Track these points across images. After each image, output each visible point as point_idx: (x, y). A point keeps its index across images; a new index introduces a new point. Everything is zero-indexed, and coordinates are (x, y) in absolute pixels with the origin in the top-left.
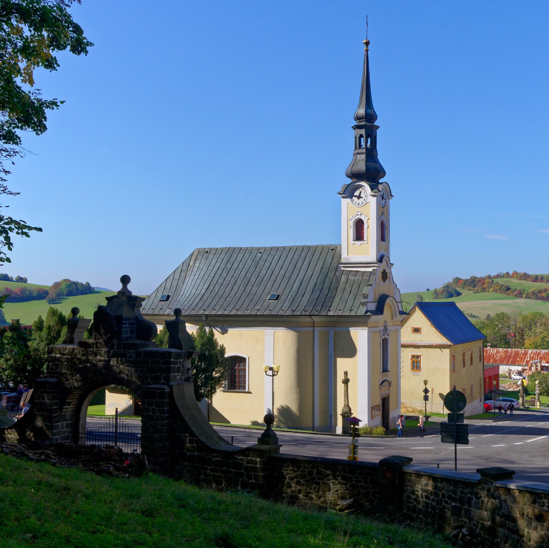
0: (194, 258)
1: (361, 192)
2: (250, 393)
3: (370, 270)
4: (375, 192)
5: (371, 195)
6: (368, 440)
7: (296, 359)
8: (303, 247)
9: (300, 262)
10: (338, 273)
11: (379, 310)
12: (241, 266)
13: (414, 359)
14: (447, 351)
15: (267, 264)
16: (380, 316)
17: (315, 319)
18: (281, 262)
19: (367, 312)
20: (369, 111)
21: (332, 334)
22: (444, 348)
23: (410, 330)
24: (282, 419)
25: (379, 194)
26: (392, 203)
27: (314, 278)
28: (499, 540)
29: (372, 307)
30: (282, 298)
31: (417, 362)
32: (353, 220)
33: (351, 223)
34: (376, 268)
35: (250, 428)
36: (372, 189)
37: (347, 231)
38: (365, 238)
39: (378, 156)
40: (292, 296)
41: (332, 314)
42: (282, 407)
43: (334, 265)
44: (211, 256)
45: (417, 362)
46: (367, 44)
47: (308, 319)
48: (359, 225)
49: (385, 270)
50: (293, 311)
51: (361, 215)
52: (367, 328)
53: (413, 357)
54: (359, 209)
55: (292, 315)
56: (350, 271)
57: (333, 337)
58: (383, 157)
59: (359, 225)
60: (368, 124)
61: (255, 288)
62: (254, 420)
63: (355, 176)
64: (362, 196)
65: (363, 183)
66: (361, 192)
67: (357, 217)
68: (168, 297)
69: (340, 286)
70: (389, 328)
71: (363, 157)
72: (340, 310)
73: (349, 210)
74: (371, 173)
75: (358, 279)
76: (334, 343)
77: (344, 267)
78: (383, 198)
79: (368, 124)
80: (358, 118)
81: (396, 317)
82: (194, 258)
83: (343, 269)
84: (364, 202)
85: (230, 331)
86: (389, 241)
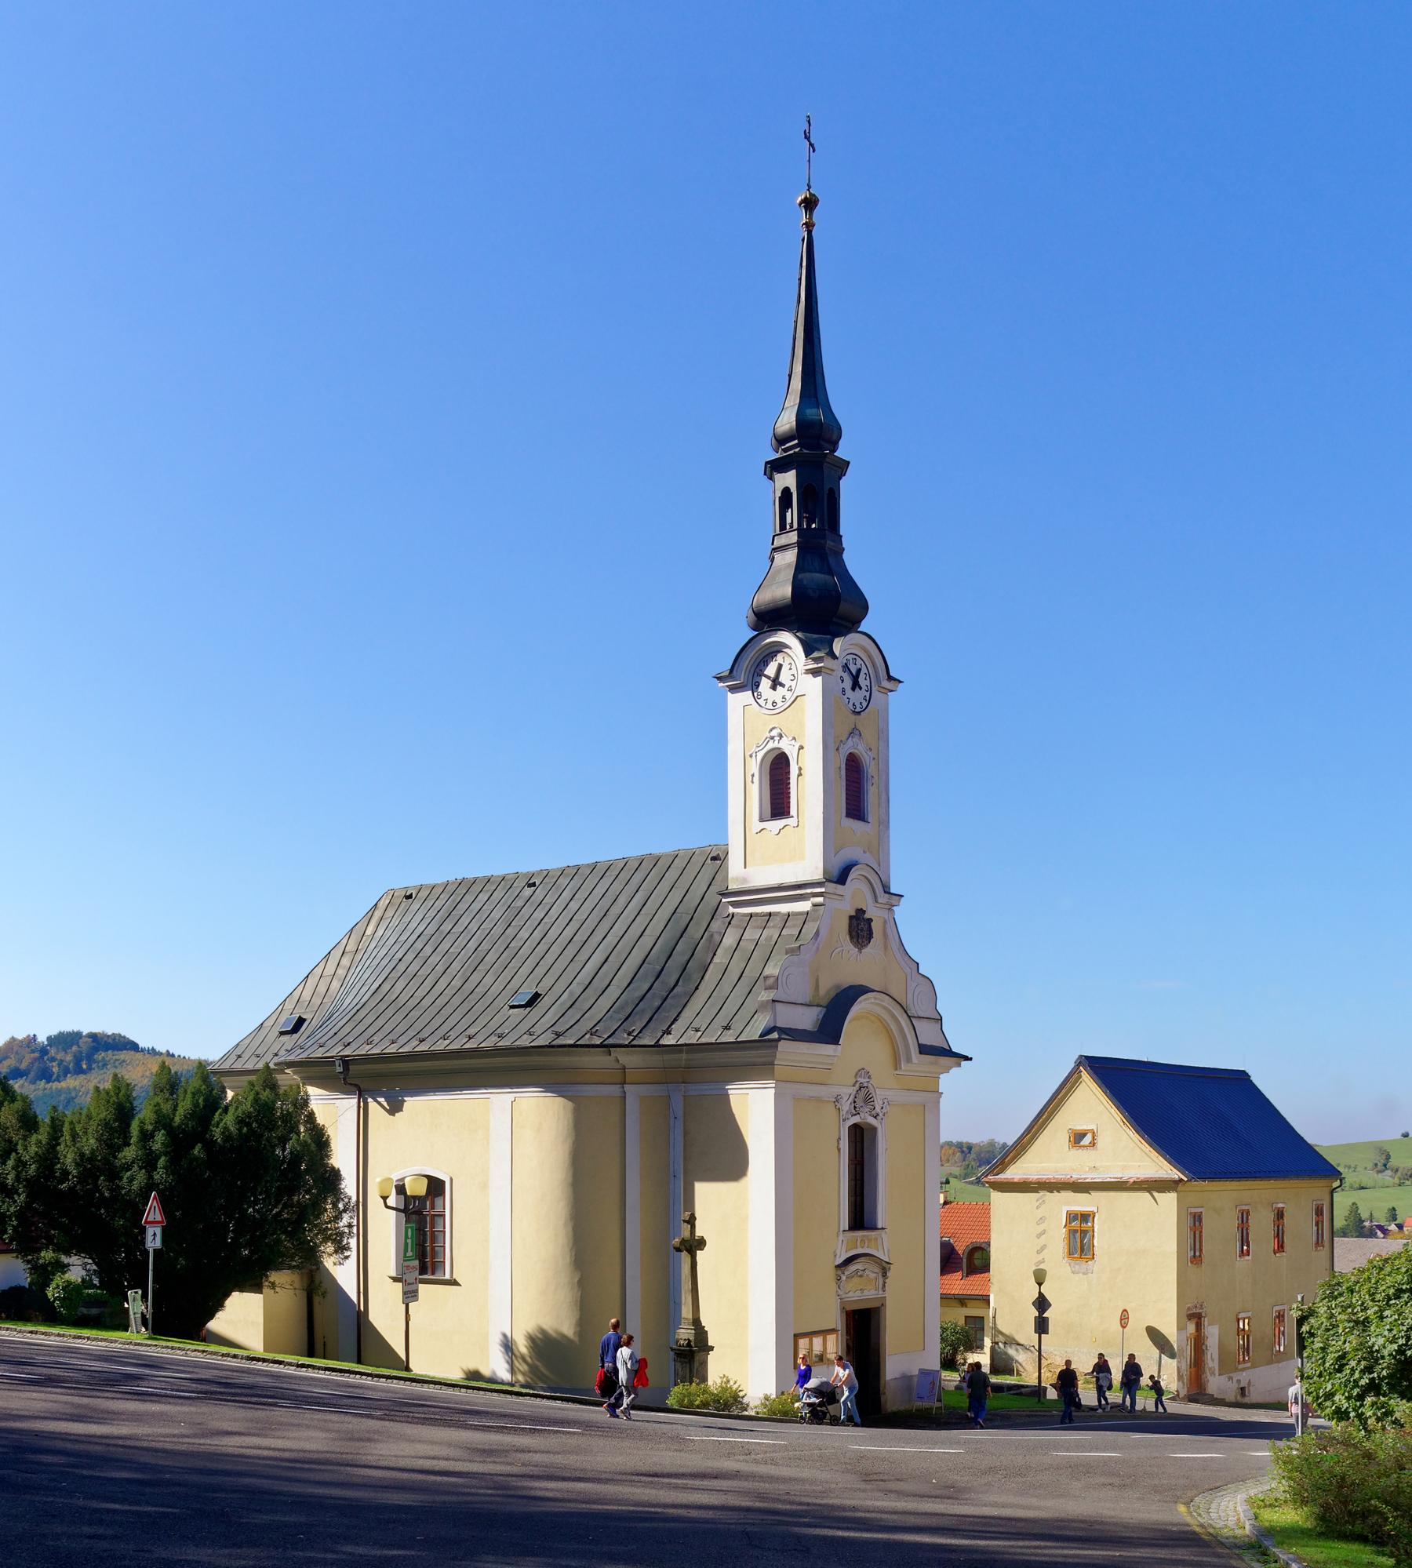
0: (378, 914)
1: (780, 666)
2: (455, 1283)
3: (805, 906)
4: (816, 660)
5: (808, 671)
6: (577, 1410)
7: (570, 1180)
9: (622, 900)
10: (716, 925)
11: (829, 1030)
12: (474, 926)
13: (1075, 1224)
14: (1169, 1200)
15: (539, 914)
16: (828, 1049)
17: (627, 1059)
18: (574, 906)
20: (811, 413)
22: (1161, 1190)
23: (1064, 1139)
24: (543, 1369)
25: (836, 665)
26: (898, 705)
27: (647, 941)
29: (807, 1019)
30: (545, 1002)
31: (1084, 1233)
32: (760, 755)
33: (754, 767)
34: (820, 900)
35: (264, 1360)
36: (808, 650)
37: (743, 789)
38: (793, 811)
39: (845, 556)
40: (571, 994)
41: (673, 1042)
42: (543, 1331)
43: (712, 898)
44: (416, 906)
45: (1084, 1233)
46: (810, 204)
47: (599, 1060)
48: (778, 770)
49: (860, 912)
50: (558, 1035)
51: (781, 736)
52: (771, 1083)
53: (1072, 1217)
54: (775, 721)
55: (550, 1046)
56: (751, 915)
57: (680, 1113)
58: (862, 555)
59: (778, 770)
60: (812, 457)
61: (489, 980)
62: (472, 1365)
63: (768, 619)
64: (782, 679)
65: (786, 637)
66: (780, 666)
67: (771, 745)
68: (301, 1021)
69: (716, 960)
71: (790, 557)
72: (697, 1030)
73: (749, 723)
74: (822, 607)
75: (769, 938)
76: (686, 1133)
77: (735, 904)
78: (856, 685)
79: (812, 457)
80: (780, 440)
81: (909, 1060)
82: (378, 914)
83: (731, 910)
84: (788, 695)
85: (412, 1103)
86: (884, 823)
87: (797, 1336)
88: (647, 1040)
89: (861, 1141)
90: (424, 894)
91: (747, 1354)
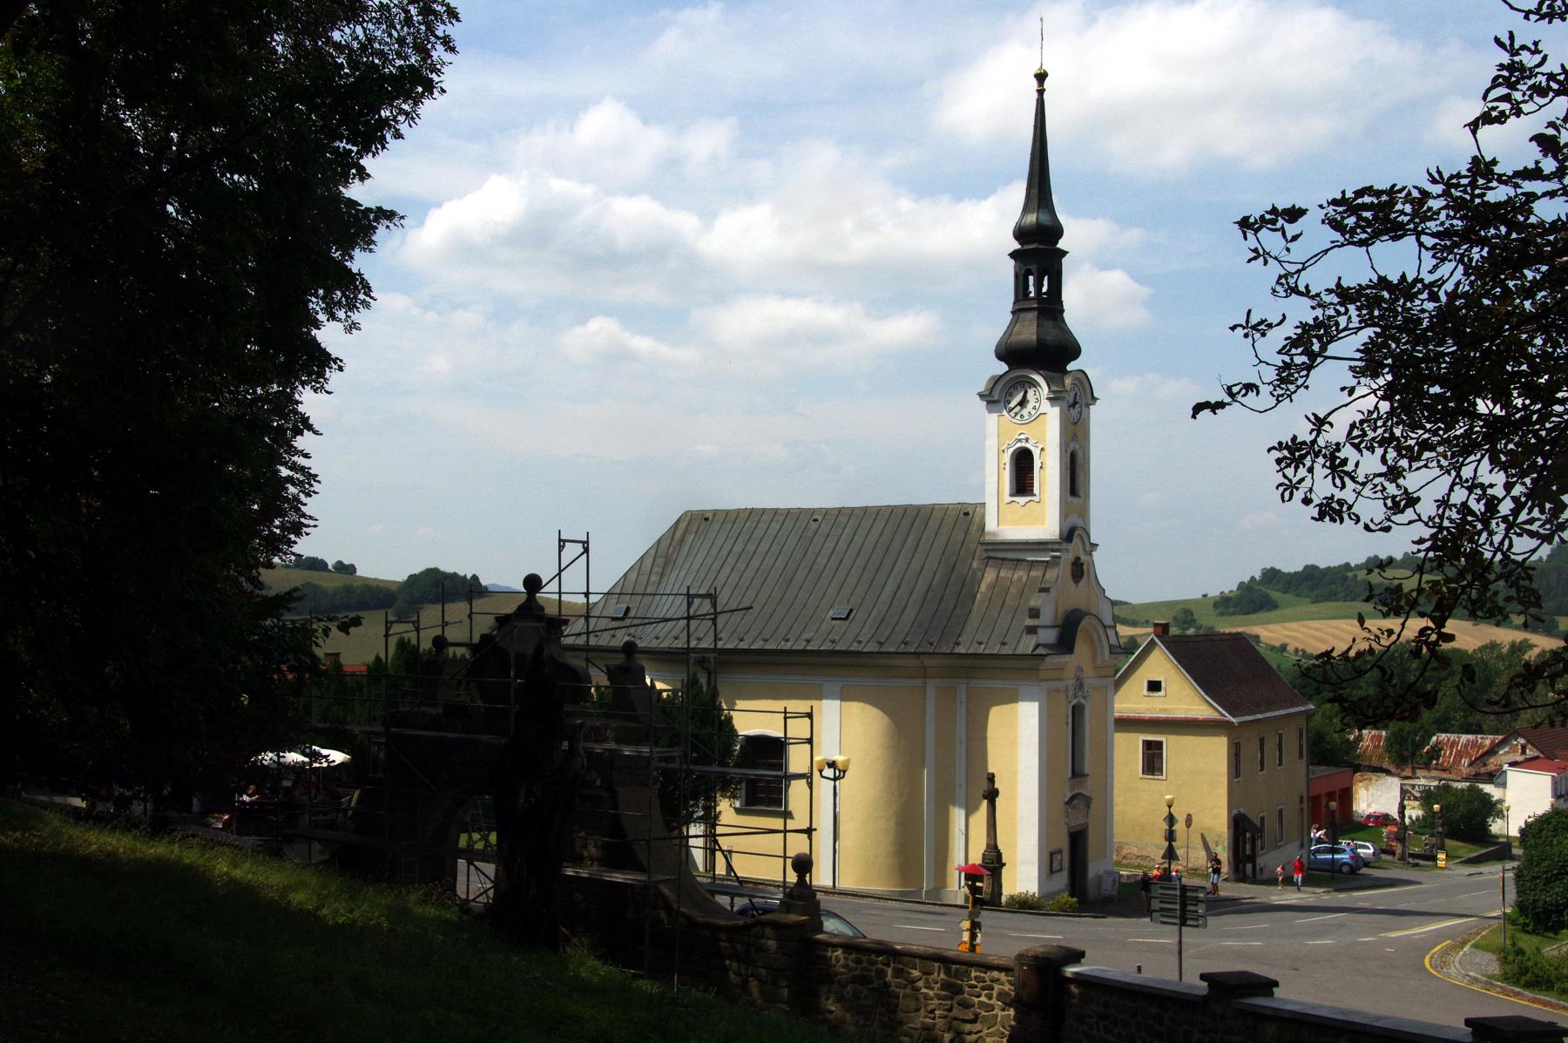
17: (928, 662)
29: (1049, 636)
38: (1036, 490)
44: (716, 527)
47: (913, 662)
49: (1078, 559)
86: (1087, 495)
87: (1052, 854)
88: (944, 650)
89: (1077, 711)
90: (721, 518)
91: (1023, 877)
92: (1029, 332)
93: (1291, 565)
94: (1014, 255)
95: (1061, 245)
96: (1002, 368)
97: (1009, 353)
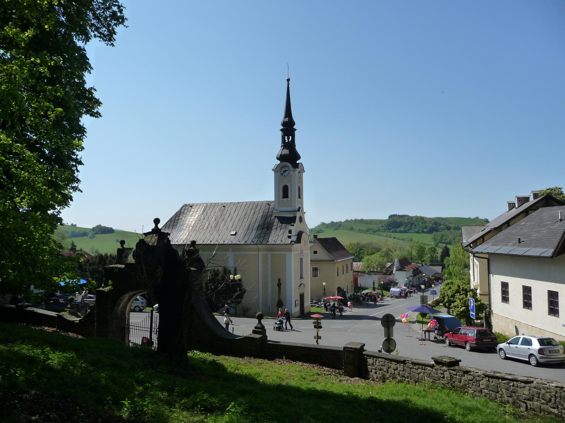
8: (250, 203)
11: (299, 241)
19: (292, 242)
21: (269, 256)
28: (275, 378)
29: (294, 238)
39: (103, 225)
46: (288, 80)
47: (255, 246)
60: (288, 128)
70: (304, 252)
79: (288, 128)
92: (286, 152)
93: (327, 222)
94: (281, 130)
95: (295, 127)
96: (279, 162)
97: (281, 158)
